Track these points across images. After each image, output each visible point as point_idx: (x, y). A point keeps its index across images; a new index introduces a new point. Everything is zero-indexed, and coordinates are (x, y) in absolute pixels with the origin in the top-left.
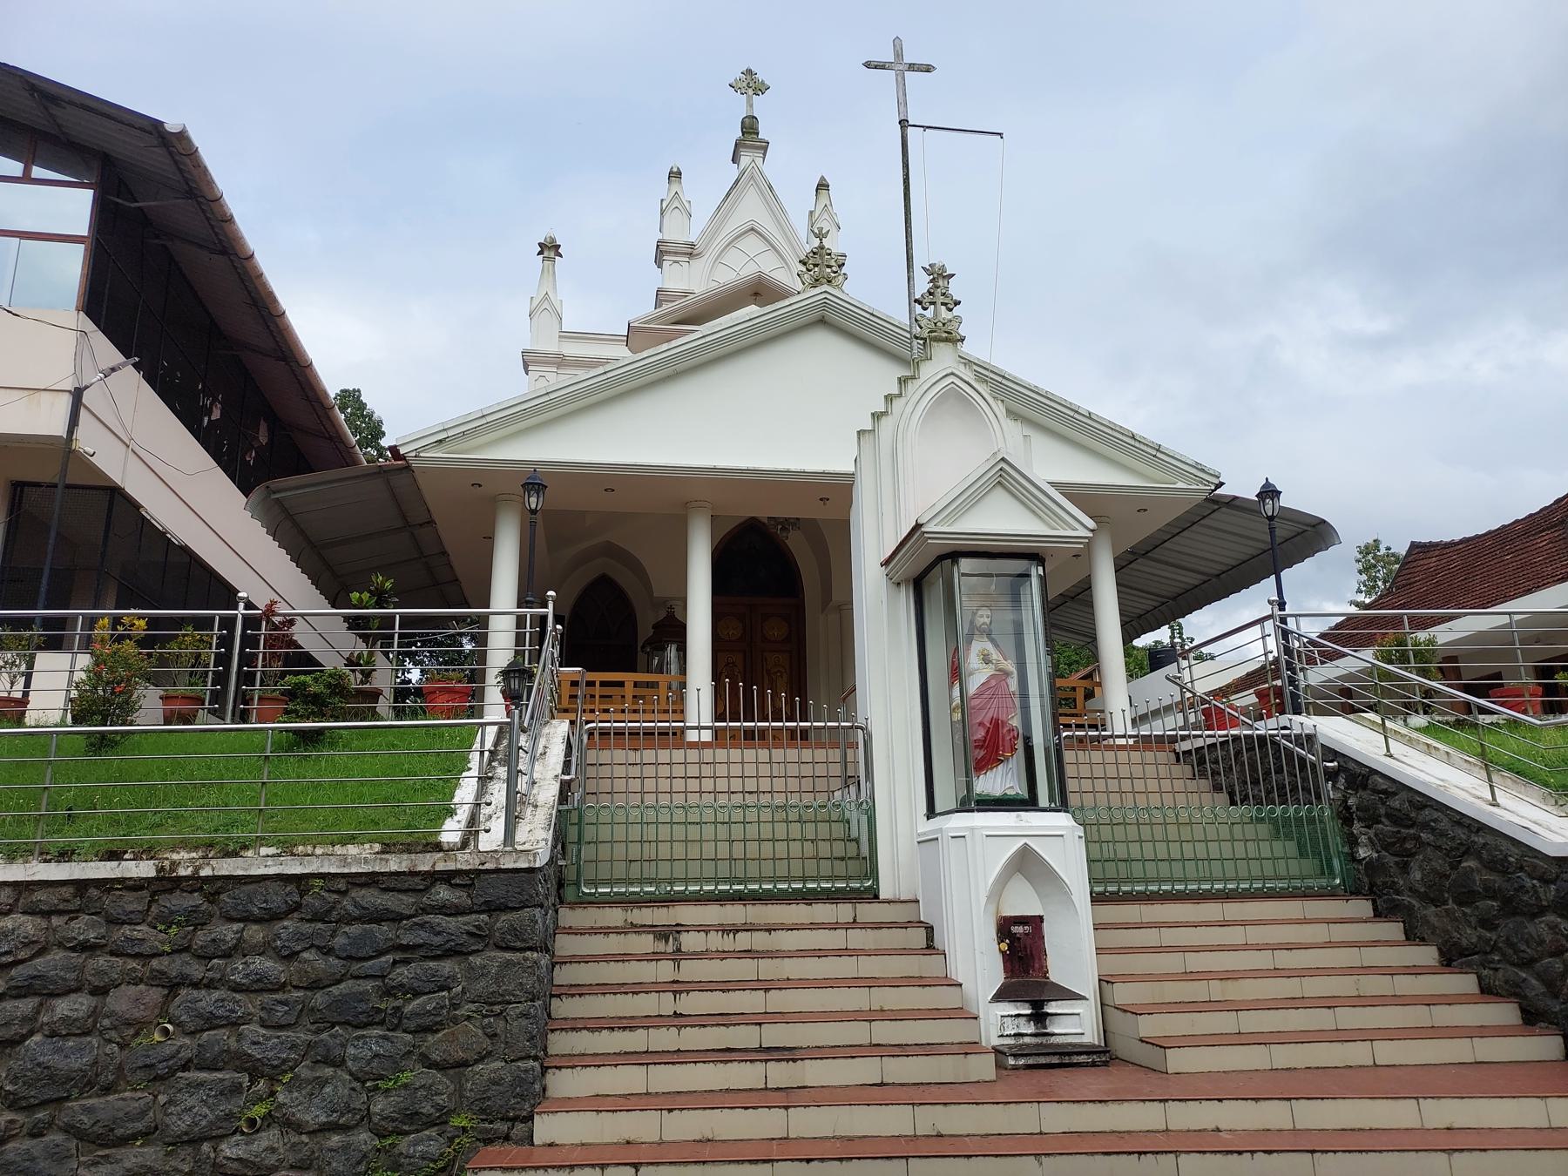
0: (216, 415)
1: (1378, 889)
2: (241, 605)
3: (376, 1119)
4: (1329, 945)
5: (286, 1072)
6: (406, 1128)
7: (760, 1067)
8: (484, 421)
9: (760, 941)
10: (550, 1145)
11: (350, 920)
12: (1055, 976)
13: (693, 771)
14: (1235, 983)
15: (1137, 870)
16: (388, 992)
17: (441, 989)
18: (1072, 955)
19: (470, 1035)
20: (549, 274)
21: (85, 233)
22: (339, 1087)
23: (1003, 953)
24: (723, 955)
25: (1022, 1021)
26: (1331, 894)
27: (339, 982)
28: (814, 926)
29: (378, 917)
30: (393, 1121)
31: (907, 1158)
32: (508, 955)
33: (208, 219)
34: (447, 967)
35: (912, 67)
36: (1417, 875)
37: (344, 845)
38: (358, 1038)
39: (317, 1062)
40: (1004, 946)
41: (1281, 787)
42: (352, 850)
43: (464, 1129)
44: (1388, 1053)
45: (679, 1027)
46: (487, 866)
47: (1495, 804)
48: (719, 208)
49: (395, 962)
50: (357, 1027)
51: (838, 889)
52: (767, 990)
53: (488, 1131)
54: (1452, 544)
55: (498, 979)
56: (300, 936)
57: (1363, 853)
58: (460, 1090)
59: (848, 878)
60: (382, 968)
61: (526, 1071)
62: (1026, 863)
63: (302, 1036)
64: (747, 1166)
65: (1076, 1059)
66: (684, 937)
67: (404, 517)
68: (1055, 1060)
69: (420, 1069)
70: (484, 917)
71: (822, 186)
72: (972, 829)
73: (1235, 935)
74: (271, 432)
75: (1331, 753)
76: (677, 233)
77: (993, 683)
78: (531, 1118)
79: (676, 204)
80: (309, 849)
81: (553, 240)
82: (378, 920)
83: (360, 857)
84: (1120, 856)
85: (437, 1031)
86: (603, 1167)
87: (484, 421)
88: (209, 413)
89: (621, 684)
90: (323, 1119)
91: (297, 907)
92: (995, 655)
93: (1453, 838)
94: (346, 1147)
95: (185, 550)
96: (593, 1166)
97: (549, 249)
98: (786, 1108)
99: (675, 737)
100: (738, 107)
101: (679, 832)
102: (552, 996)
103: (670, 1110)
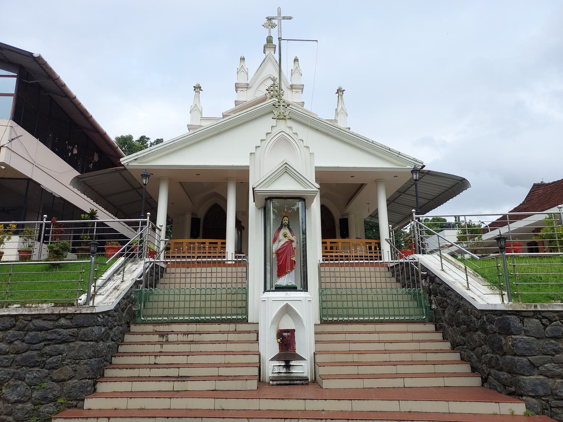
0: (75, 152)
1: (434, 318)
2: (45, 219)
3: (33, 399)
4: (412, 341)
5: (5, 382)
6: (43, 402)
7: (172, 383)
8: (151, 152)
9: (196, 337)
10: (89, 409)
11: (32, 330)
12: (297, 352)
13: (204, 275)
14: (363, 355)
15: (366, 311)
16: (42, 355)
17: (59, 354)
18: (305, 344)
19: (68, 370)
20: (197, 97)
21: (14, 93)
22: (22, 388)
23: (279, 343)
24: (183, 342)
25: (281, 367)
26: (423, 322)
27: (26, 352)
28: (220, 332)
29: (41, 329)
30: (39, 400)
31: (202, 417)
32: (82, 343)
33: (58, 86)
34: (62, 347)
35: (284, 18)
36: (447, 315)
37: (42, 303)
38: (30, 371)
39: (16, 379)
40: (279, 340)
41: (413, 281)
42: (45, 306)
43: (62, 404)
44: (410, 382)
45: (150, 368)
46: (77, 312)
47: (468, 289)
48: (258, 70)
49: (45, 345)
50: (30, 367)
51: (233, 319)
52: (188, 356)
53: (70, 404)
54: (549, 184)
55: (78, 351)
56: (14, 336)
57: (434, 306)
58: (62, 390)
59: (237, 315)
60: (40, 347)
61: (85, 383)
62: (287, 310)
63: (12, 370)
64: (146, 419)
65: (295, 382)
66: (169, 336)
67: (131, 186)
68: (288, 382)
69: (50, 382)
70: (76, 330)
71: (296, 60)
72: (268, 298)
73: (375, 337)
74: (100, 157)
75: (424, 269)
76: (243, 80)
77: (286, 244)
78: (83, 400)
79: (242, 70)
80: (31, 305)
81: (199, 85)
82: (41, 330)
83: (46, 308)
84: (345, 306)
85: (57, 369)
86: (98, 418)
87: (151, 152)
88: (72, 151)
89: (217, 243)
90: (16, 399)
91: (14, 326)
92: (289, 234)
93: (455, 302)
94: (23, 409)
95: (61, 198)
96: (94, 418)
97: (198, 88)
98: (171, 398)
99: (223, 264)
100: (265, 33)
101: (187, 298)
102: (112, 356)
103: (131, 398)
